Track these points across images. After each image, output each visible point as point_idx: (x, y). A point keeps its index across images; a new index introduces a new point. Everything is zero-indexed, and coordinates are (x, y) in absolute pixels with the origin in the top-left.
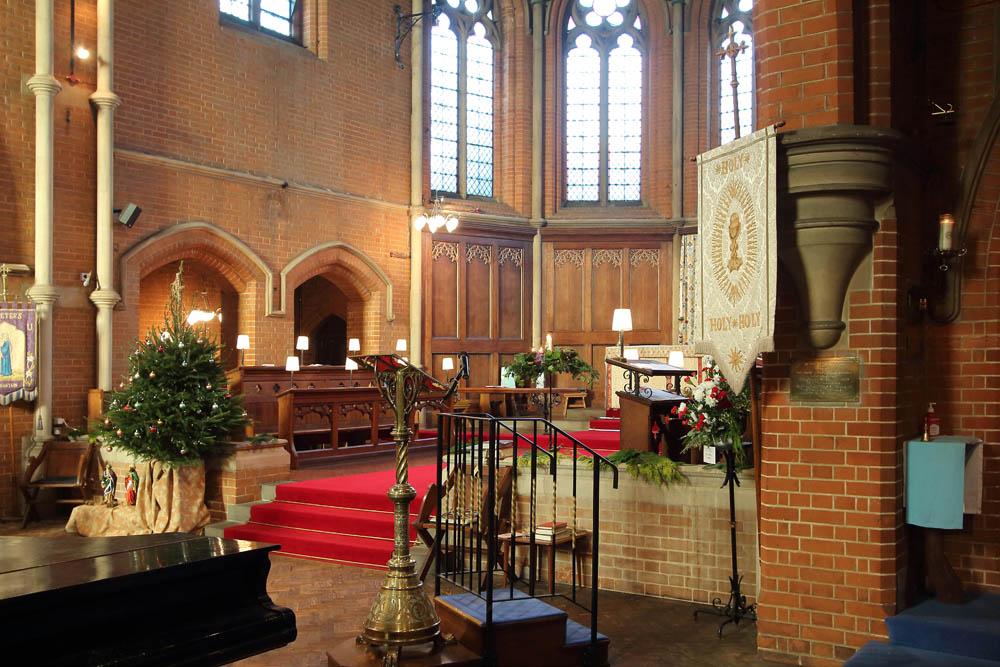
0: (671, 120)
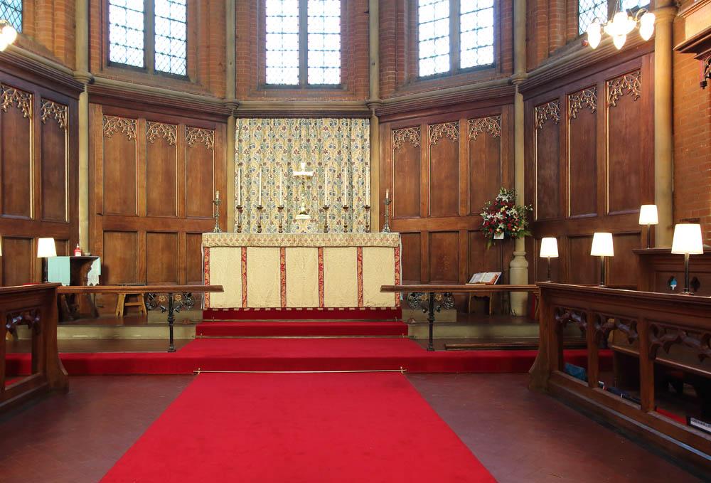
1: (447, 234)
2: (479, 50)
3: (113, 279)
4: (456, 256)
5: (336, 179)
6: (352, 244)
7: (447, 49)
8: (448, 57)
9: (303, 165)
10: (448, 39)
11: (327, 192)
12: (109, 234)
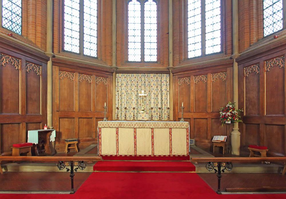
0: (112, 25)
1: (202, 119)
2: (214, 46)
3: (64, 137)
4: (206, 128)
5: (156, 97)
6: (167, 127)
7: (200, 47)
8: (201, 50)
9: (143, 92)
10: (200, 43)
11: (152, 102)
12: (62, 119)
